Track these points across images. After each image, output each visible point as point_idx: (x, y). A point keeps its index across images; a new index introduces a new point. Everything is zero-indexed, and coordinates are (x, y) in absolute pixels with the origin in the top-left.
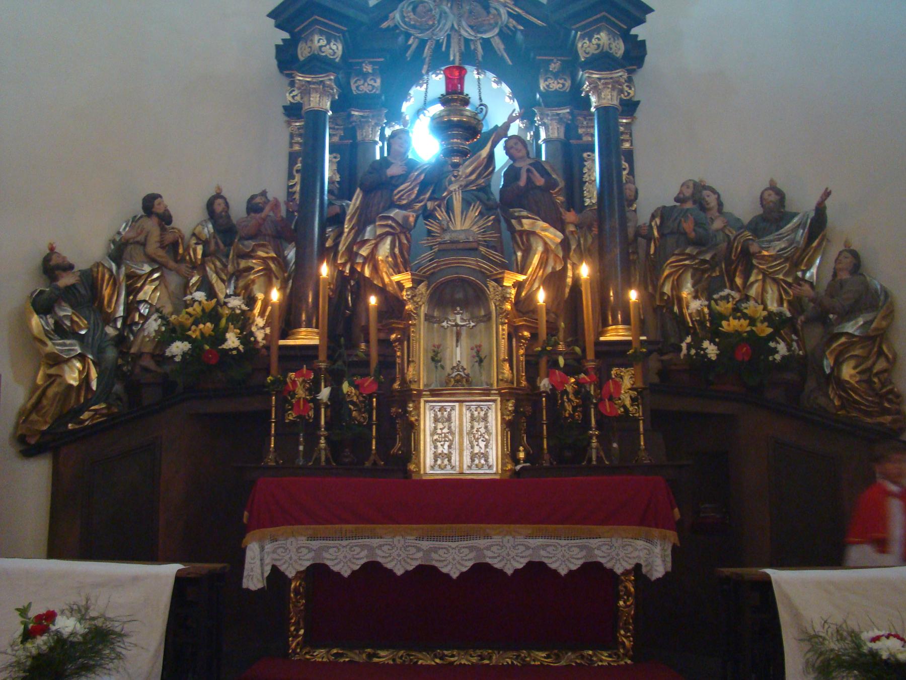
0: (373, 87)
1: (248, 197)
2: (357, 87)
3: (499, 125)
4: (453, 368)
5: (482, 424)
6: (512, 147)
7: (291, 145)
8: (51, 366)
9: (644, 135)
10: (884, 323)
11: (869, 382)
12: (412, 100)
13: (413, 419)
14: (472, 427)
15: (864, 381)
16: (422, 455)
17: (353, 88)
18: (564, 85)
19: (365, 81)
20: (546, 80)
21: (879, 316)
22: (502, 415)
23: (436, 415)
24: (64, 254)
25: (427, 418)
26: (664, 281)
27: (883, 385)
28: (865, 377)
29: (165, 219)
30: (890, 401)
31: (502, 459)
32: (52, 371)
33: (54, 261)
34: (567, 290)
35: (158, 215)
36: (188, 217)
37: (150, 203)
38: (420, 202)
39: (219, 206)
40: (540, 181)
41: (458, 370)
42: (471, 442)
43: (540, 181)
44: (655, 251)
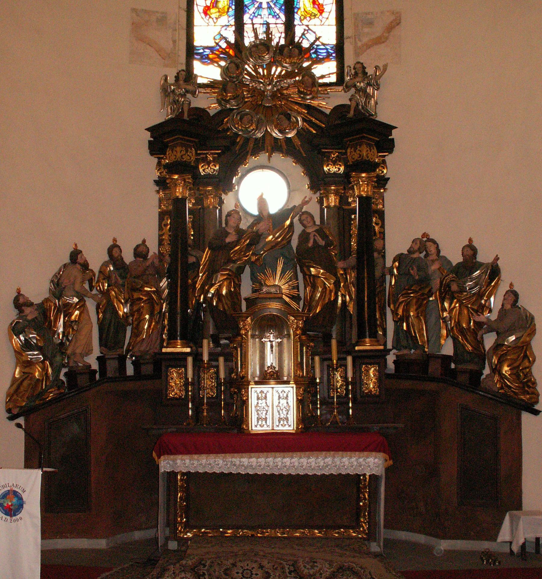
0: (214, 170)
1: (135, 246)
2: (204, 170)
3: (297, 205)
4: (268, 367)
5: (285, 401)
6: (304, 220)
7: (160, 207)
8: (26, 367)
9: (393, 202)
10: (528, 339)
11: (518, 376)
12: (240, 174)
13: (244, 398)
14: (279, 403)
15: (515, 374)
16: (250, 420)
17: (201, 170)
18: (339, 169)
19: (209, 166)
20: (327, 166)
21: (526, 334)
22: (297, 396)
23: (258, 396)
24: (27, 295)
25: (254, 392)
26: (399, 305)
27: (526, 376)
28: (515, 371)
29: (85, 266)
30: (529, 387)
31: (297, 422)
32: (27, 370)
33: (21, 300)
34: (338, 311)
35: (80, 264)
36: (96, 259)
37: (75, 255)
38: (247, 257)
39: (115, 251)
40: (322, 243)
41: (271, 369)
42: (279, 412)
43: (322, 243)
44: (395, 283)
